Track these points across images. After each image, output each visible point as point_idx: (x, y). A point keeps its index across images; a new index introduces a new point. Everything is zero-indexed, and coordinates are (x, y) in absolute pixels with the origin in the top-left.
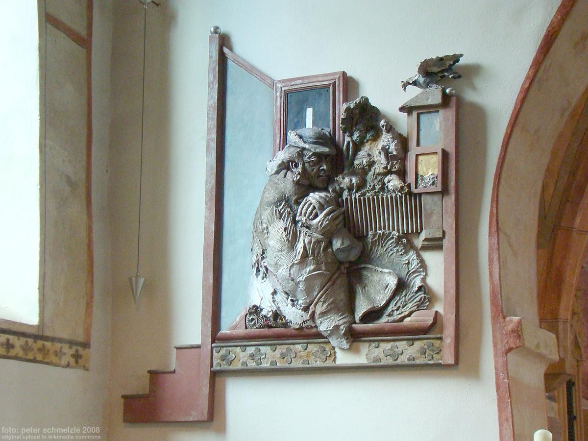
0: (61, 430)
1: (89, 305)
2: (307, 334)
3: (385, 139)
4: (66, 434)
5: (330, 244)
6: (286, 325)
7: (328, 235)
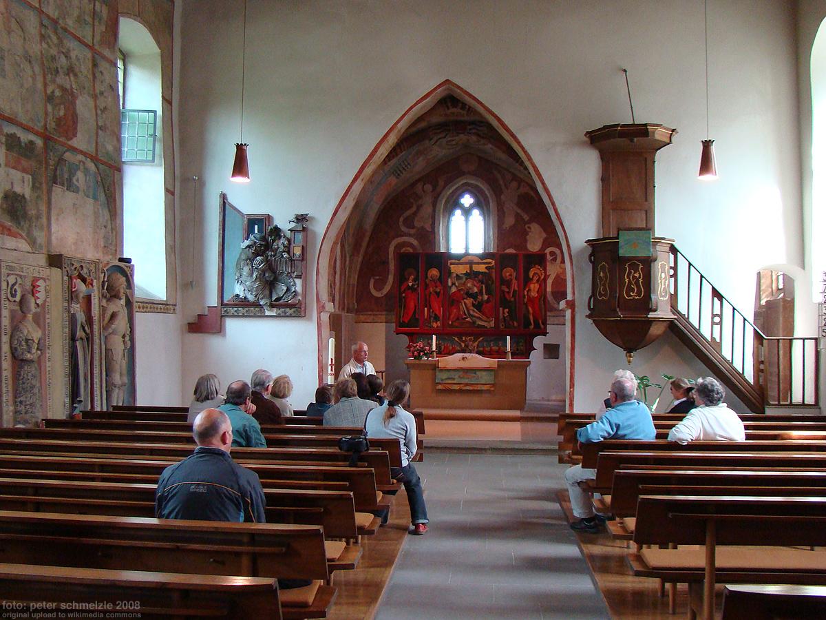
0: (86, 606)
1: (176, 291)
2: (256, 304)
3: (282, 240)
4: (93, 612)
5: (264, 275)
6: (248, 301)
7: (264, 272)
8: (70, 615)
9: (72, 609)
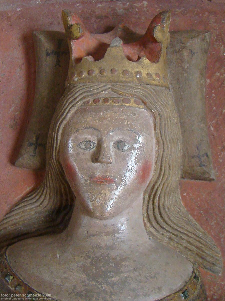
0: (31, 295)
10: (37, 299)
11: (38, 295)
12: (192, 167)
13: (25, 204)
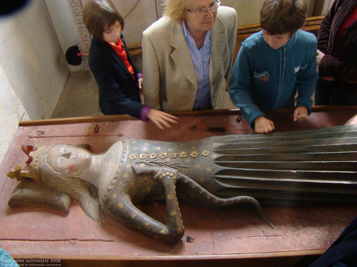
0: (37, 261)
8: (30, 265)
9: (41, 262)
10: (44, 265)
11: (44, 261)
12: (122, 186)
13: (86, 208)
